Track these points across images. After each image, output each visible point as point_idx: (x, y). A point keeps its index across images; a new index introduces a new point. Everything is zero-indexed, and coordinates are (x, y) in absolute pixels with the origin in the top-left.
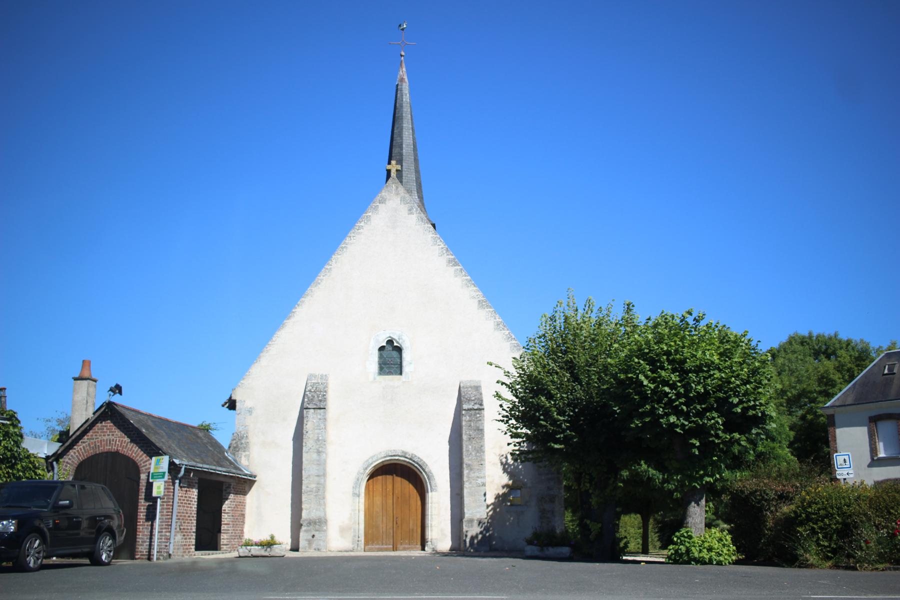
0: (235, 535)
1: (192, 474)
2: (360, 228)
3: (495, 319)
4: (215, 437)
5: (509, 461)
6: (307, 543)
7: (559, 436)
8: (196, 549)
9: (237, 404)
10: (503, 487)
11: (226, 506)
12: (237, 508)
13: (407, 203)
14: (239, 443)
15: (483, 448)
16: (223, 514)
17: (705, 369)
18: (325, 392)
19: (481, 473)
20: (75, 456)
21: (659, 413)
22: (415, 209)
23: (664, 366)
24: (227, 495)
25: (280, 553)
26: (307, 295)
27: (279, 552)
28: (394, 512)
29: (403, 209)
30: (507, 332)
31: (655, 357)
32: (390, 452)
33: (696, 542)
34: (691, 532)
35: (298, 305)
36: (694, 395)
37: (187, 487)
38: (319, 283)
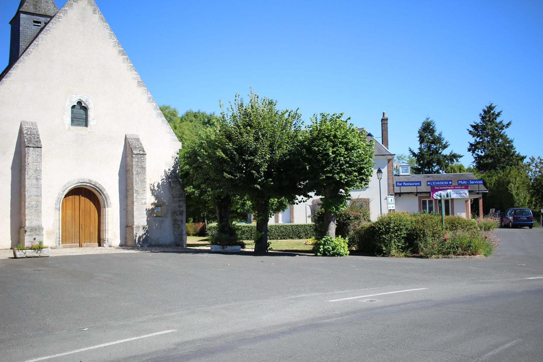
3: (148, 95)
5: (155, 188)
10: (152, 204)
18: (38, 135)
19: (144, 196)
22: (97, 11)
26: (20, 62)
30: (155, 104)
38: (30, 54)
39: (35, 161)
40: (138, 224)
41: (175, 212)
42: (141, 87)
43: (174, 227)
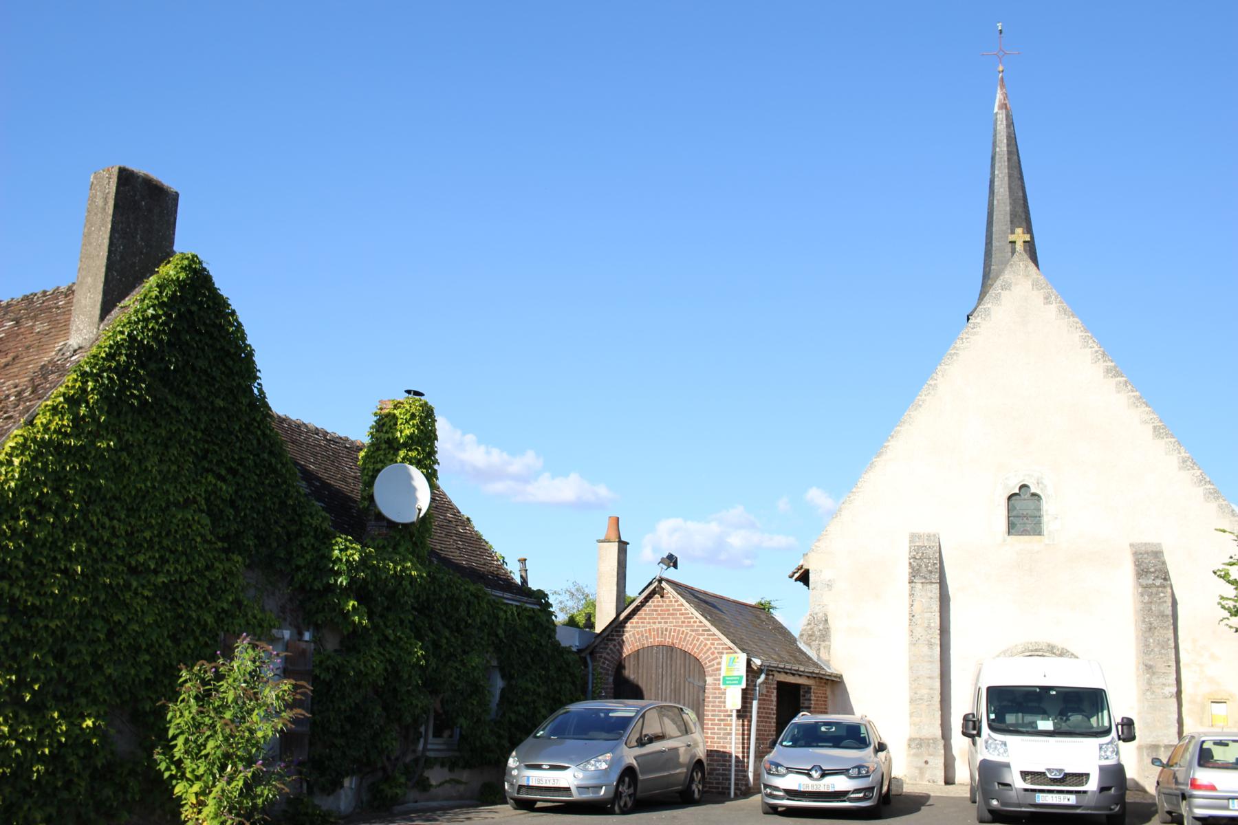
3: (1180, 453)
14: (815, 629)
20: (615, 650)
29: (1037, 297)
30: (1198, 473)
32: (1029, 645)
35: (892, 437)
38: (920, 406)
42: (1163, 438)
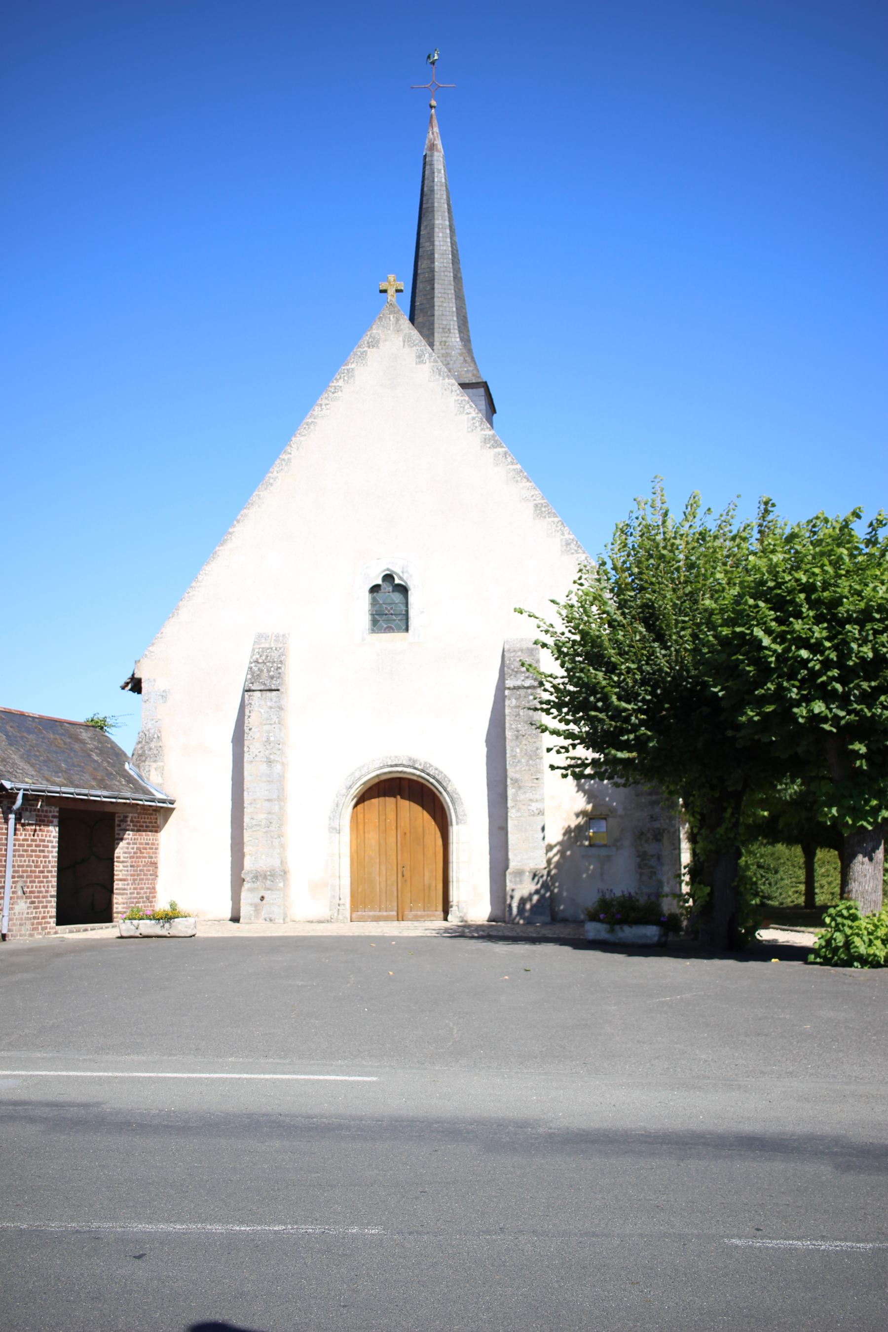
0: (138, 896)
1: (40, 803)
2: (337, 389)
3: (563, 534)
4: (113, 738)
6: (253, 909)
7: (626, 737)
8: (59, 923)
9: (143, 685)
10: (577, 815)
11: (121, 851)
12: (141, 853)
13: (415, 345)
14: (146, 748)
15: (539, 751)
16: (115, 864)
17: (877, 616)
21: (791, 697)
22: (427, 355)
23: (802, 612)
24: (121, 833)
25: (186, 932)
27: (184, 929)
28: (399, 857)
31: (785, 594)
33: (863, 927)
34: (856, 909)
35: (238, 521)
36: (856, 664)
37: (36, 825)
38: (271, 484)
39: (264, 722)
40: (519, 864)
41: (642, 833)
43: (641, 874)
